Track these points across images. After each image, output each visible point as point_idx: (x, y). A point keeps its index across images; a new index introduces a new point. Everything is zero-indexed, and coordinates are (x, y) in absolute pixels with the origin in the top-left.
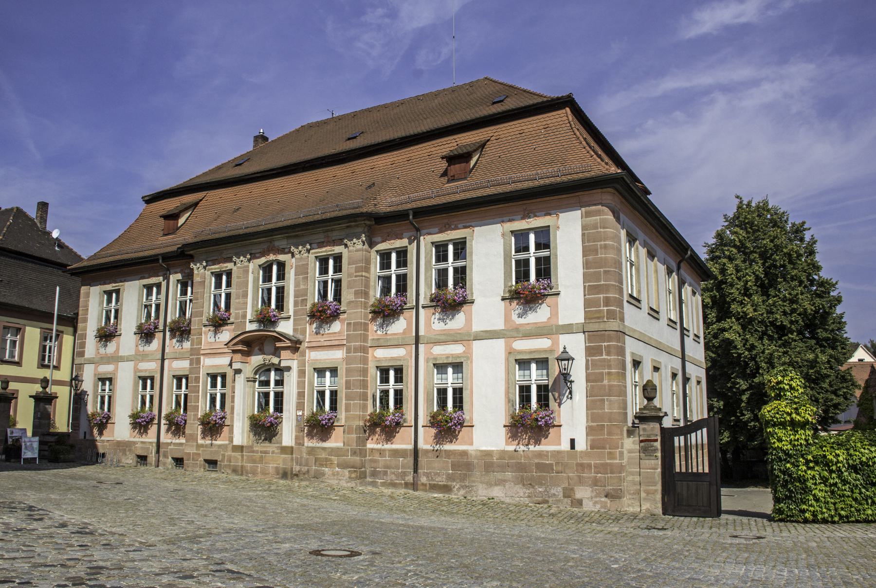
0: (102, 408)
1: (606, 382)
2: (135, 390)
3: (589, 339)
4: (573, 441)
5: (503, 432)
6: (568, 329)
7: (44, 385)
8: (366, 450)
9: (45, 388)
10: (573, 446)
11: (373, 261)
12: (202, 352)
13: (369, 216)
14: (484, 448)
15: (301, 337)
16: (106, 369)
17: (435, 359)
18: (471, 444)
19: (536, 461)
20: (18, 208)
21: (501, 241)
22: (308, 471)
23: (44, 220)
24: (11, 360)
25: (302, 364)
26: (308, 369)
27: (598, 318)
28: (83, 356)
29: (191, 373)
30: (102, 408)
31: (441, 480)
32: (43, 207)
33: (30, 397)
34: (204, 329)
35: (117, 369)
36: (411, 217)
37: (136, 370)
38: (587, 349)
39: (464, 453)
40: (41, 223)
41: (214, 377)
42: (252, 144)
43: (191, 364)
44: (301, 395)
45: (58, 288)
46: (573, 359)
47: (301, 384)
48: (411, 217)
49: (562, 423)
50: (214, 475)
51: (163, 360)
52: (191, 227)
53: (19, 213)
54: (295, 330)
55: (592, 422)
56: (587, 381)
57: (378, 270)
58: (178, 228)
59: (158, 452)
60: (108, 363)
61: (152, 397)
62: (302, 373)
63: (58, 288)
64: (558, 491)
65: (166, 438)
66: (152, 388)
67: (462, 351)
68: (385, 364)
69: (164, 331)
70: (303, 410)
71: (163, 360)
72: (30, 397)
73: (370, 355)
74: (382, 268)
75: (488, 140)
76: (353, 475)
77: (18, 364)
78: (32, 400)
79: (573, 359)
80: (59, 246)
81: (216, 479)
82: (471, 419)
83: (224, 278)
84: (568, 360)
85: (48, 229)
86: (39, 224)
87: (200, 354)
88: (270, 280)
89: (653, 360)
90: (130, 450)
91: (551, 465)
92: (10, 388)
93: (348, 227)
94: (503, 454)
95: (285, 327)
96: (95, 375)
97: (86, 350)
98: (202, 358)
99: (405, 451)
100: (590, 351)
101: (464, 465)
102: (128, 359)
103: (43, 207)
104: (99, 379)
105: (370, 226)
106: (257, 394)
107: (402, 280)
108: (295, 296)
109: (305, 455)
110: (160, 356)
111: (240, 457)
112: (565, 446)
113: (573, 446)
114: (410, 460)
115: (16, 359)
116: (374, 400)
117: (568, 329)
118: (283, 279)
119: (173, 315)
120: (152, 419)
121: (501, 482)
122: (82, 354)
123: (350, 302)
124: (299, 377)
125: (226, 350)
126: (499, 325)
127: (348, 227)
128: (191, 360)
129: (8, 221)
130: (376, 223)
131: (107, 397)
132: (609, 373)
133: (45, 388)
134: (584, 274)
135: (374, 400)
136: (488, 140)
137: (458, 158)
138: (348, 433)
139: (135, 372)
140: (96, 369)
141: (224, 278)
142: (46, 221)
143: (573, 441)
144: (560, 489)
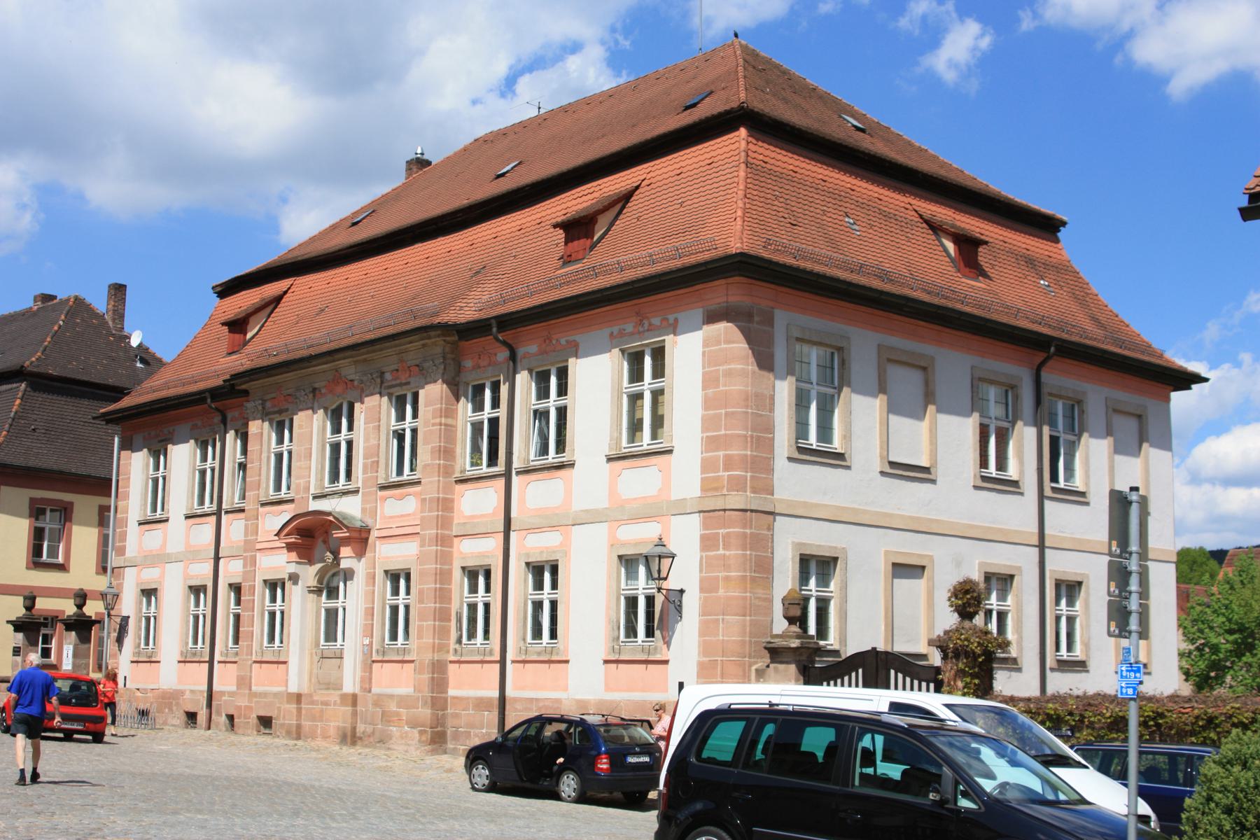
1: (721, 592)
3: (705, 525)
7: (79, 601)
8: (446, 700)
9: (80, 606)
12: (259, 546)
13: (446, 328)
14: (579, 697)
15: (369, 522)
17: (528, 555)
18: (566, 689)
20: (76, 298)
22: (373, 733)
23: (119, 315)
26: (380, 575)
27: (716, 489)
28: (123, 554)
32: (118, 291)
33: (8, 622)
34: (261, 509)
35: (163, 575)
36: (494, 330)
37: (186, 576)
40: (114, 320)
41: (472, 574)
42: (404, 174)
43: (245, 566)
45: (116, 439)
48: (494, 330)
50: (268, 739)
51: (217, 559)
52: (271, 340)
53: (79, 306)
54: (364, 510)
56: (702, 590)
57: (470, 414)
58: (246, 343)
59: (209, 705)
60: (153, 566)
61: (487, 606)
63: (116, 439)
66: (488, 590)
67: (558, 543)
68: (470, 563)
71: (217, 559)
72: (8, 622)
73: (455, 550)
74: (539, 398)
75: (637, 188)
76: (424, 738)
77: (62, 568)
80: (143, 361)
81: (268, 747)
82: (566, 650)
83: (648, 361)
85: (127, 330)
86: (110, 323)
88: (547, 396)
89: (887, 552)
90: (178, 704)
92: (37, 606)
93: (424, 346)
97: (128, 544)
98: (258, 555)
99: (491, 699)
100: (707, 542)
103: (118, 291)
104: (143, 591)
105: (453, 343)
108: (365, 457)
109: (370, 708)
110: (501, 527)
111: (294, 711)
115: (61, 560)
116: (459, 620)
117: (680, 509)
118: (663, 376)
123: (426, 466)
124: (367, 584)
125: (278, 544)
127: (424, 346)
128: (245, 559)
129: (56, 322)
130: (460, 339)
131: (201, 618)
132: (727, 579)
133: (80, 606)
135: (459, 620)
136: (637, 188)
137: (578, 228)
138: (420, 673)
139: (185, 579)
141: (648, 361)
142: (122, 317)
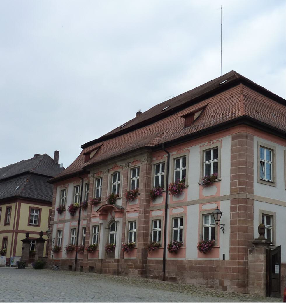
0: (94, 242)
1: (237, 225)
2: (70, 236)
4: (224, 255)
5: (196, 250)
6: (223, 198)
10: (224, 258)
11: (153, 169)
13: (149, 148)
15: (124, 207)
16: (60, 226)
19: (209, 266)
21: (200, 155)
24: (35, 224)
25: (124, 219)
26: (127, 223)
27: (236, 192)
29: (87, 226)
30: (94, 242)
31: (173, 275)
33: (21, 241)
38: (231, 208)
39: (182, 261)
43: (87, 222)
44: (123, 234)
46: (221, 213)
47: (124, 229)
48: (163, 147)
49: (220, 246)
54: (122, 204)
55: (232, 246)
61: (160, 232)
62: (124, 224)
64: (217, 282)
65: (168, 257)
66: (160, 227)
68: (155, 219)
69: (167, 191)
70: (124, 242)
78: (22, 242)
79: (221, 213)
84: (221, 213)
87: (91, 217)
91: (215, 268)
94: (197, 262)
95: (119, 203)
96: (57, 229)
100: (232, 209)
101: (182, 268)
102: (194, 203)
104: (58, 231)
106: (83, 237)
107: (216, 165)
112: (221, 258)
113: (224, 258)
114: (161, 266)
119: (171, 180)
120: (158, 246)
121: (195, 277)
122: (53, 219)
126: (197, 198)
128: (87, 220)
134: (231, 169)
138: (139, 252)
140: (70, 224)
143: (224, 255)
144: (218, 281)
